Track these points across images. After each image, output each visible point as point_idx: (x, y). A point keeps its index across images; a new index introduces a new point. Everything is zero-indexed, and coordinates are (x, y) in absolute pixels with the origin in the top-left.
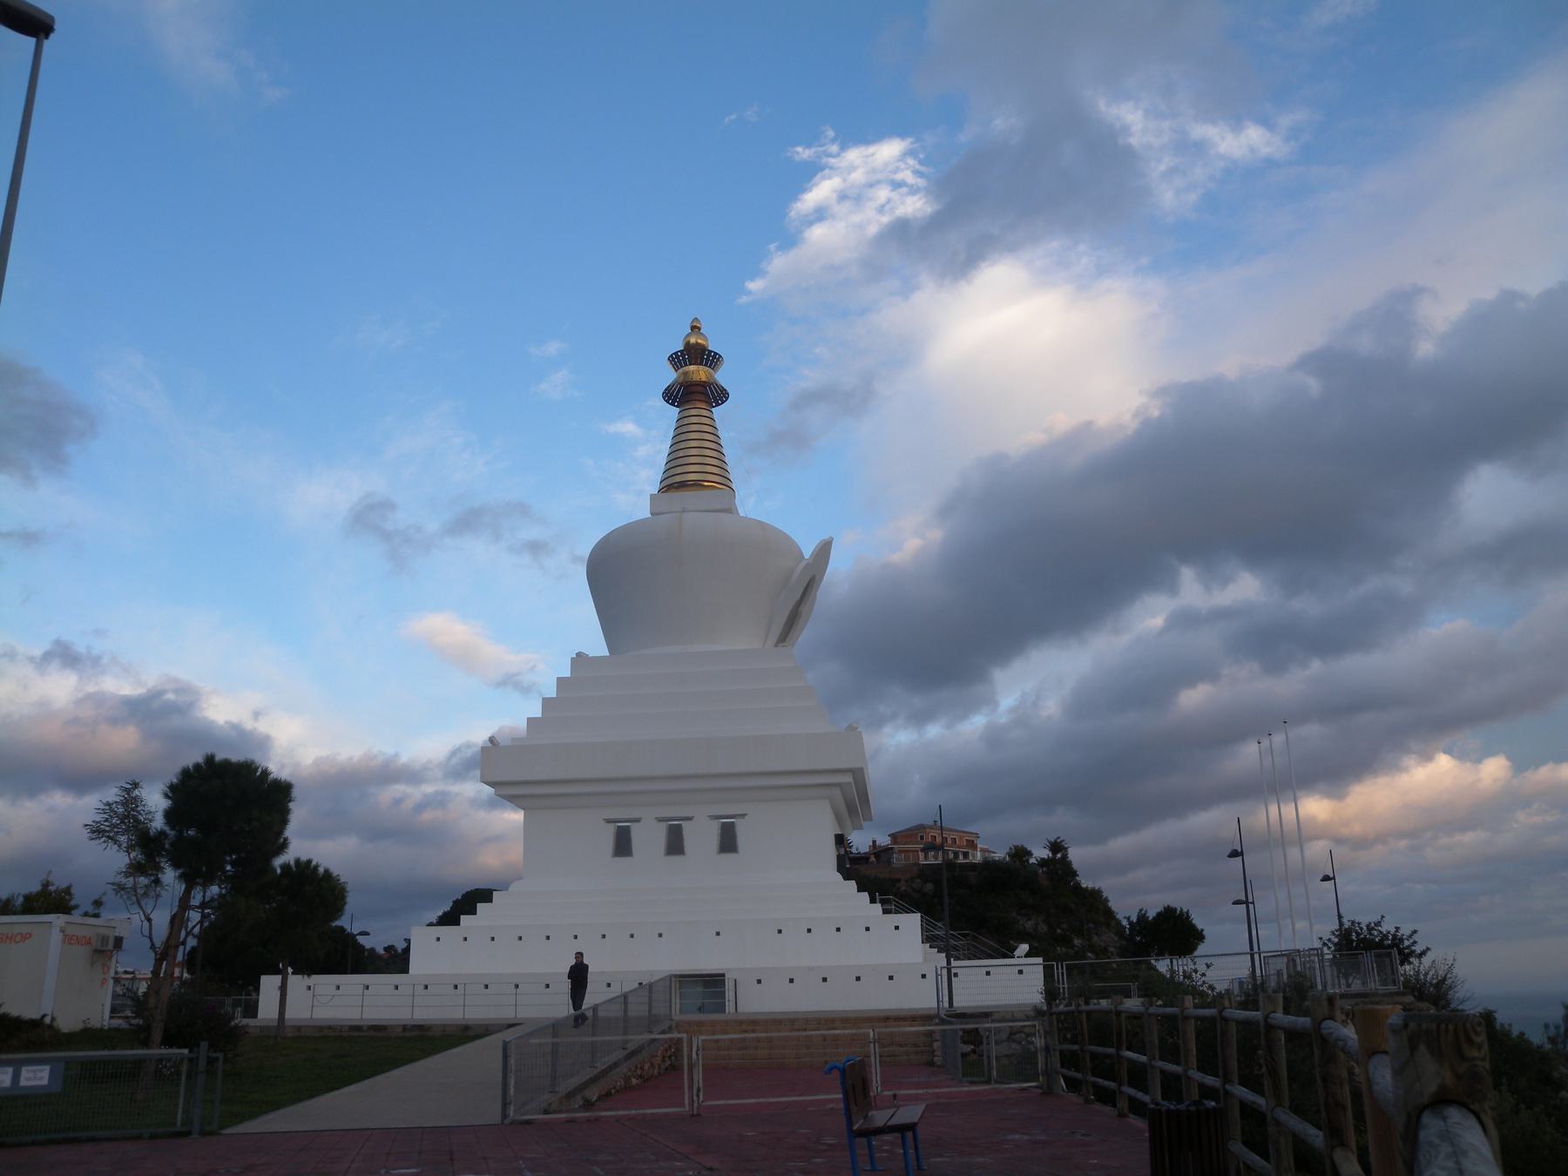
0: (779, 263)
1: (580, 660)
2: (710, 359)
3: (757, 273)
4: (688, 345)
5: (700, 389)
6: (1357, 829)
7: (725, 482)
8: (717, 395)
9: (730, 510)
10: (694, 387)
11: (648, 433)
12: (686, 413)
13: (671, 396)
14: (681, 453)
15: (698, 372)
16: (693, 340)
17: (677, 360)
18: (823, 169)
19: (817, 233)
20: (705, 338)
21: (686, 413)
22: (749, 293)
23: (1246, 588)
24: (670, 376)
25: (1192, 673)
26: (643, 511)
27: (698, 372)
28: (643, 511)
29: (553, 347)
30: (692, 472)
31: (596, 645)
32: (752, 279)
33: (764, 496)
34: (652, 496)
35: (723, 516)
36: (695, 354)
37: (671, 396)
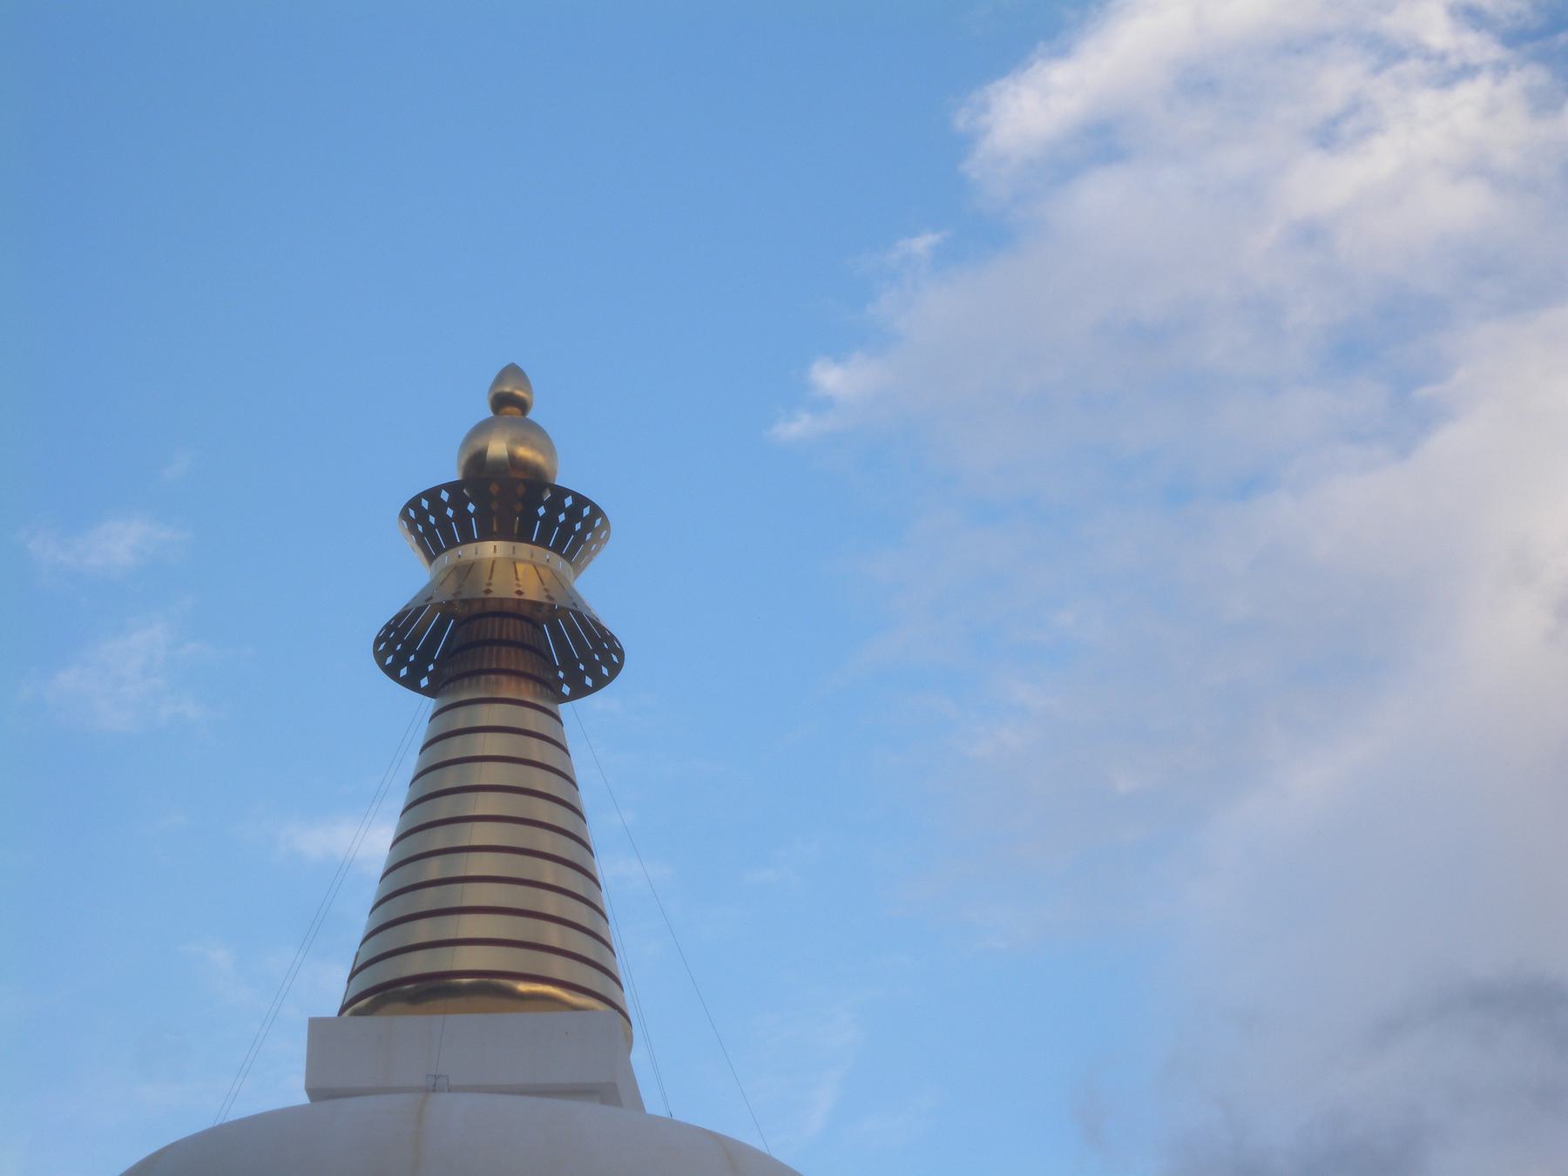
4: (477, 465)
5: (512, 629)
6: (531, 685)
7: (594, 983)
8: (572, 654)
9: (611, 1089)
10: (497, 628)
12: (461, 718)
13: (411, 649)
14: (434, 869)
15: (508, 566)
16: (497, 448)
19: (1098, 197)
20: (547, 446)
21: (461, 718)
22: (823, 405)
24: (404, 576)
27: (508, 566)
28: (284, 1085)
29: (120, 543)
34: (317, 1026)
35: (585, 1112)
36: (506, 495)
37: (411, 649)
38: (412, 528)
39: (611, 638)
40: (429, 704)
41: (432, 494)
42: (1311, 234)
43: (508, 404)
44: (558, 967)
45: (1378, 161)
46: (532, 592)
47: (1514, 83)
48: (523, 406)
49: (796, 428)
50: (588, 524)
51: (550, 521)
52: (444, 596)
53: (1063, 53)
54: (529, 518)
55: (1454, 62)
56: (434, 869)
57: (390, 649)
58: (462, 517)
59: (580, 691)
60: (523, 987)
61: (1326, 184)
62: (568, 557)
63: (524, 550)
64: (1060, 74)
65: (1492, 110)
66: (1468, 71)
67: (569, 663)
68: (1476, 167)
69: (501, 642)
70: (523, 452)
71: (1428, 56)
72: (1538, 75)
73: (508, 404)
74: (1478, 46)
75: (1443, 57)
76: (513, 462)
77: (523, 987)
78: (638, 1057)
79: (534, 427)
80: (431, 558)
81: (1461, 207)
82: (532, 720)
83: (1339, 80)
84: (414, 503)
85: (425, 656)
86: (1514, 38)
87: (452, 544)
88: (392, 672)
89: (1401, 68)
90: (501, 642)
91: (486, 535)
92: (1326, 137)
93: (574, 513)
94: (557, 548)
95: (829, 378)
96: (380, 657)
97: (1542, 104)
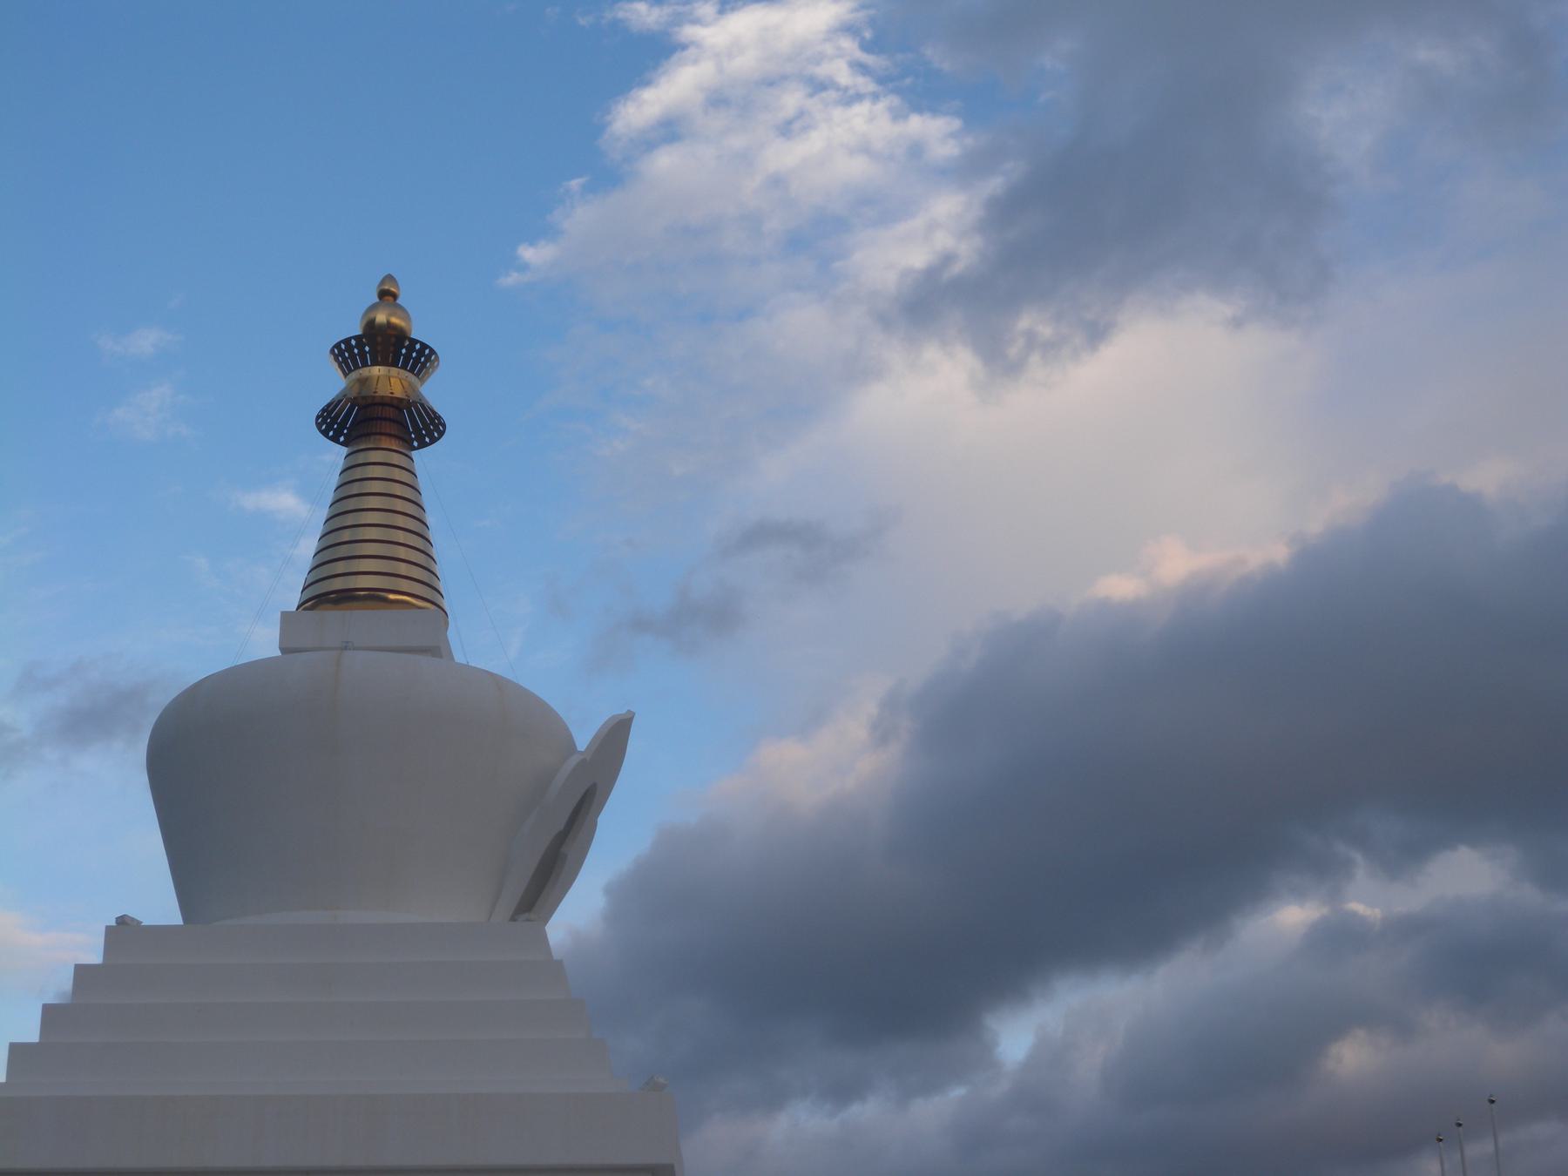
0: (583, 217)
1: (123, 932)
2: (418, 358)
3: (541, 232)
4: (370, 326)
5: (390, 412)
7: (429, 596)
8: (422, 426)
9: (437, 650)
10: (380, 408)
11: (294, 493)
12: (361, 458)
14: (346, 535)
15: (388, 380)
16: (381, 318)
17: (348, 354)
18: (684, 47)
19: (665, 161)
20: (407, 317)
21: (361, 458)
22: (524, 267)
23: (1469, 877)
24: (332, 383)
25: (1339, 1019)
26: (264, 642)
27: (388, 380)
28: (264, 642)
29: (146, 341)
30: (367, 573)
31: (159, 905)
32: (532, 242)
33: (507, 622)
34: (285, 616)
36: (384, 344)
38: (336, 359)
39: (439, 418)
40: (344, 450)
41: (347, 341)
42: (777, 182)
43: (387, 295)
44: (405, 585)
45: (813, 143)
46: (398, 393)
47: (881, 106)
48: (395, 296)
49: (511, 279)
50: (428, 358)
51: (408, 357)
52: (353, 394)
53: (647, 83)
54: (397, 354)
55: (851, 92)
56: (346, 535)
57: (324, 421)
58: (362, 354)
59: (423, 445)
60: (392, 596)
61: (784, 156)
62: (417, 375)
63: (394, 371)
64: (648, 95)
65: (871, 119)
66: (859, 97)
67: (417, 430)
68: (864, 148)
69: (381, 419)
70: (394, 320)
71: (837, 88)
72: (895, 100)
73: (387, 295)
74: (865, 84)
75: (846, 89)
76: (389, 325)
77: (392, 596)
78: (451, 634)
79: (400, 307)
80: (346, 375)
81: (855, 169)
82: (396, 458)
83: (791, 100)
84: (337, 346)
85: (343, 425)
86: (882, 80)
87: (357, 367)
88: (325, 433)
89: (824, 95)
90: (381, 419)
91: (375, 363)
92: (787, 129)
93: (421, 353)
94: (412, 371)
95: (528, 253)
96: (319, 426)
97: (897, 116)
